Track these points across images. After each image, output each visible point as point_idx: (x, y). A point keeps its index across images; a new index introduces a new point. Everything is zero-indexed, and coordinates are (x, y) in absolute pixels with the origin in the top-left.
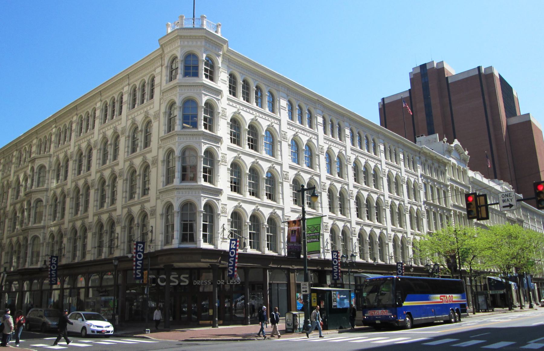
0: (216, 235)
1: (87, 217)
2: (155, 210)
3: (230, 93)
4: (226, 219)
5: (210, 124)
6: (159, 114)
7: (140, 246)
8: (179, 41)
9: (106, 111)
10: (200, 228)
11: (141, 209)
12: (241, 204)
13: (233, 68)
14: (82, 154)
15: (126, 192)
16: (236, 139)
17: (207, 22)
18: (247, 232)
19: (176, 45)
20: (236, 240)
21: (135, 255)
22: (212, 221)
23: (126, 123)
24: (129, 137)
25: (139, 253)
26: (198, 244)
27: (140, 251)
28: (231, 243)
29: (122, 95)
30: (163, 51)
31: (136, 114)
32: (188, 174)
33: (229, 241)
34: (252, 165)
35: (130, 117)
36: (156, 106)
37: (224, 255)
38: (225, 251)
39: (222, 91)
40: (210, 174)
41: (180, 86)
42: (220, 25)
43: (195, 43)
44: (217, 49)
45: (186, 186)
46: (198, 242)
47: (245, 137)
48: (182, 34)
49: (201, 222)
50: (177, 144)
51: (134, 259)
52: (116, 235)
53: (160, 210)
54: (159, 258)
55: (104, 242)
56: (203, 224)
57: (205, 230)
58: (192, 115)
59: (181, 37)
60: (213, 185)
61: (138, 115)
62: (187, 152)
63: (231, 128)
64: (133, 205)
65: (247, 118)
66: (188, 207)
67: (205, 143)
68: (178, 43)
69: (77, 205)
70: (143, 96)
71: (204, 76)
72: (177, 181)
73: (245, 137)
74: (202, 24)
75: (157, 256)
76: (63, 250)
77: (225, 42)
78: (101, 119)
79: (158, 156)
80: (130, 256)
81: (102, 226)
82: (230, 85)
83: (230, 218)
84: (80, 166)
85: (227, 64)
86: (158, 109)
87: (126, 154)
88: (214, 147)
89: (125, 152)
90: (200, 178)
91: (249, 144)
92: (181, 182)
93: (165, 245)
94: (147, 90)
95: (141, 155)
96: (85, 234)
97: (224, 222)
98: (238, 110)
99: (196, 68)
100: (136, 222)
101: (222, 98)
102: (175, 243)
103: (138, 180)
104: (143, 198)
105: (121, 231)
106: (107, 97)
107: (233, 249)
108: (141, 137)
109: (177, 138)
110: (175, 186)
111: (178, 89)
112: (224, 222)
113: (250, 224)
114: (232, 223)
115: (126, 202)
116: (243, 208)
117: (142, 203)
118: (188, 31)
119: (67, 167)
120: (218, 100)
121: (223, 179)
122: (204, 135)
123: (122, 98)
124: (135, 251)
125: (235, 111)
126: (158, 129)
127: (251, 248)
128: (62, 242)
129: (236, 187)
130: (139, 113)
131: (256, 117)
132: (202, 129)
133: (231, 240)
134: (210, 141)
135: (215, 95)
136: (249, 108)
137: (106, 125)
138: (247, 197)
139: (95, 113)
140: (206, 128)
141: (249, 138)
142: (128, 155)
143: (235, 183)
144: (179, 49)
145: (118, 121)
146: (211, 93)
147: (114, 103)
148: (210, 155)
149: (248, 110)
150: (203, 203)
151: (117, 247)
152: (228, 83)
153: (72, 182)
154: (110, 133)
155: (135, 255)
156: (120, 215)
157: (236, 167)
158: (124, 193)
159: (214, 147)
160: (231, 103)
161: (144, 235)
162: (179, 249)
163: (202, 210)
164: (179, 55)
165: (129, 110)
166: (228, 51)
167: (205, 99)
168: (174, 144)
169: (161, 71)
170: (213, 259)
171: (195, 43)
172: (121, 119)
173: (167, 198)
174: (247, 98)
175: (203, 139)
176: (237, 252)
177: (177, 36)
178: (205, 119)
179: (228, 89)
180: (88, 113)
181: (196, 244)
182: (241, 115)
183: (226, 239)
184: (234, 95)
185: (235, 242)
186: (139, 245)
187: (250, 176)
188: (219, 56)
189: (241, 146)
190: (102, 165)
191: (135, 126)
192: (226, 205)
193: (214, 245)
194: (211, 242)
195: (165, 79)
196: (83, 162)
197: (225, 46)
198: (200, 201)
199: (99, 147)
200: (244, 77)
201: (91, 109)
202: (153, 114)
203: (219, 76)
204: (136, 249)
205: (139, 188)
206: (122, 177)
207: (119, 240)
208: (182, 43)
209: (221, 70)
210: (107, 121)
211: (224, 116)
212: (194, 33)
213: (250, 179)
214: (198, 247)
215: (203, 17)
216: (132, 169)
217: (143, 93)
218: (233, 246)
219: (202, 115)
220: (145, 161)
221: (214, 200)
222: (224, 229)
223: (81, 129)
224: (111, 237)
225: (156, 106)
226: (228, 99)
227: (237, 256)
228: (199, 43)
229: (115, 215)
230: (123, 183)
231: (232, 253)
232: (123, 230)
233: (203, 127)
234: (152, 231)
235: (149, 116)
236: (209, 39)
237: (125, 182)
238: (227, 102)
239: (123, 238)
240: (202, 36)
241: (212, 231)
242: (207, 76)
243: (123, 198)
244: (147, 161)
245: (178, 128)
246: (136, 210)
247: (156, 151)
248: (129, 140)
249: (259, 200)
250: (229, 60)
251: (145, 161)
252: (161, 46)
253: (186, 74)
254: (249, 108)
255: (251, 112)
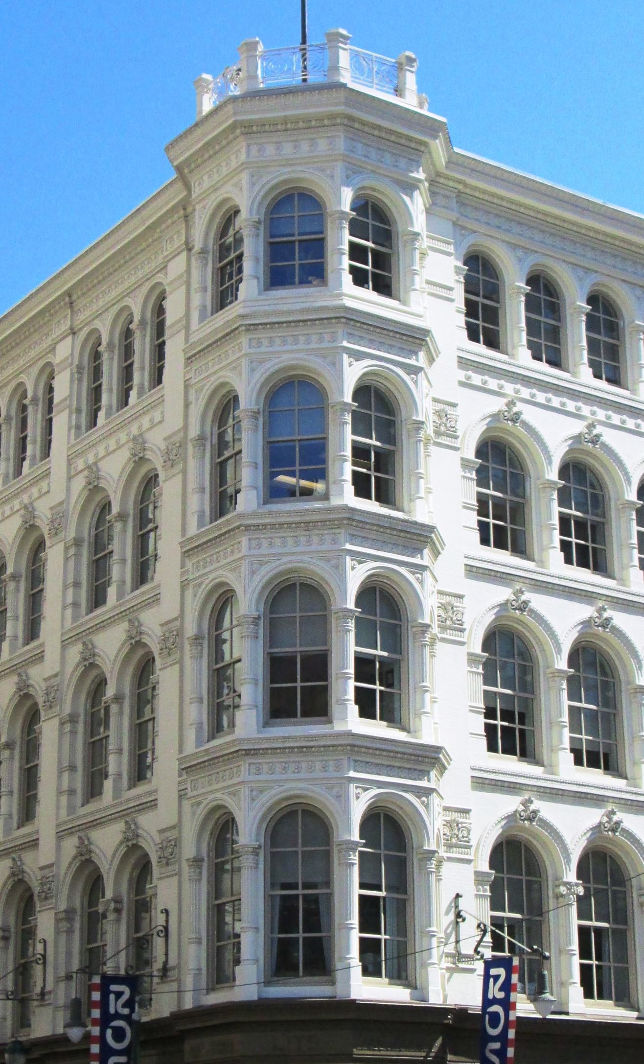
0: (420, 943)
1: (34, 844)
2: (176, 843)
3: (473, 336)
4: (468, 871)
5: (379, 475)
6: (182, 445)
7: (119, 995)
8: (242, 143)
9: (97, 373)
10: (348, 916)
11: (13, 874)
12: (536, 804)
13: (482, 229)
14: (106, 507)
15: (72, 768)
16: (504, 525)
17: (355, 56)
18: (566, 926)
19: (234, 164)
20: (506, 963)
21: (96, 1031)
22: (401, 882)
23: (68, 490)
24: (78, 542)
25: (116, 1023)
26: (339, 985)
27: (117, 1016)
28: (487, 976)
29: (162, 297)
30: (188, 187)
31: (101, 450)
32: (297, 689)
33: (480, 966)
34: (581, 634)
35: (80, 464)
36: (170, 413)
37: (459, 1027)
38: (461, 1013)
39: (427, 332)
40: (385, 687)
41: (252, 328)
42: (410, 61)
43: (305, 147)
44: (402, 163)
45: (285, 738)
46: (339, 975)
47: (546, 514)
48: (252, 120)
49: (350, 890)
50: (245, 566)
51: (95, 1049)
52: (160, 920)
53: (192, 843)
54: (188, 1045)
55: (110, 951)
56: (362, 898)
57: (369, 921)
58: (310, 440)
59: (248, 129)
60: (404, 729)
61: (108, 454)
62: (296, 599)
63: (482, 482)
64: (96, 824)
65: (552, 434)
66: (299, 828)
67: (361, 558)
68: (240, 153)
69: (96, 751)
70: (127, 373)
71: (347, 278)
72: (247, 721)
73: (546, 514)
74: (335, 68)
75: (184, 1035)
76: (38, 969)
77: (433, 128)
78: (79, 411)
79: (182, 616)
80: (75, 1034)
81: (95, 884)
82: (468, 303)
83: (484, 867)
84: (100, 568)
85: (454, 215)
86: (180, 424)
87: (69, 612)
88: (403, 570)
89: (64, 608)
90: (343, 703)
91: (565, 547)
92: (266, 725)
93: (210, 989)
94: (142, 346)
95: (121, 616)
96: (25, 921)
97: (455, 894)
98: (511, 404)
99: (316, 247)
100: (109, 894)
101: (431, 360)
102: (248, 983)
103: (112, 718)
104: (135, 792)
105: (57, 932)
106: (129, 293)
107: (495, 1001)
108: (124, 545)
109: (244, 540)
110: (241, 741)
111: (244, 339)
112: (455, 894)
113: (581, 891)
114: (496, 887)
115: (71, 809)
116: (544, 823)
117: (128, 815)
118: (273, 102)
119: (36, 578)
120: (415, 371)
121: (449, 700)
122: (354, 523)
123: (160, 311)
124: (96, 1013)
125: (494, 409)
126: (180, 506)
127: (588, 994)
128: (28, 934)
129: (511, 730)
130: (112, 443)
131: (591, 426)
132: (348, 497)
133: (489, 965)
134: (382, 545)
135: (401, 351)
136: (558, 390)
137: (23, 481)
138: (562, 776)
139: (50, 390)
140: (362, 490)
141: (564, 520)
142: (75, 618)
143: (507, 715)
144: (245, 177)
145: (36, 481)
146: (380, 346)
147: (128, 333)
148: (384, 605)
149: (556, 402)
150: (358, 808)
151: (43, 994)
152: (459, 295)
153: (65, 645)
154: (114, 469)
155: (96, 1031)
156: (51, 866)
157: (508, 651)
158: (66, 776)
159: (403, 570)
160: (477, 379)
161: (140, 945)
162: (262, 1006)
163: (355, 836)
164: (247, 200)
165: (77, 436)
166: (454, 161)
167: (352, 373)
168: (235, 568)
169: (188, 271)
170: (410, 1046)
171: (305, 147)
172: (47, 474)
173: (214, 791)
174: (548, 345)
175: (353, 538)
176: (512, 1016)
177: (233, 127)
178: (360, 453)
179: (462, 319)
180: (126, 314)
181: (333, 983)
182: (525, 425)
183: (470, 958)
184: (492, 342)
185: (501, 971)
186: (114, 988)
187: (572, 681)
188: (410, 187)
189: (530, 558)
190: (90, 610)
191: (98, 498)
192: (466, 812)
193: (410, 985)
194: (400, 974)
195: (202, 298)
196: (115, 546)
197: (437, 146)
198: (343, 799)
199: (71, 534)
200: (531, 261)
201: (35, 370)
202: (163, 446)
203: (414, 273)
204: (104, 1004)
205: (120, 751)
206: (57, 709)
207: (50, 969)
208: (254, 150)
209: (424, 243)
210: (101, 415)
211: (447, 433)
212: (296, 108)
213: (573, 695)
214: (339, 992)
215: (334, 39)
216: (94, 673)
217: (125, 361)
218: (495, 992)
219: (344, 438)
220: (136, 643)
221: (409, 796)
222: (458, 915)
223: (96, 393)
224: (137, 929)
225: (170, 413)
226: (464, 363)
227: (512, 1034)
228: (322, 145)
229: (33, 864)
230: (61, 734)
231: (495, 1017)
232: (64, 925)
233: (349, 488)
234: (166, 928)
235: (149, 455)
236: (364, 123)
237: (67, 728)
238: (461, 375)
239: (62, 957)
240: (332, 116)
241: (402, 928)
242: (359, 278)
243: (60, 793)
244: (146, 639)
245: (248, 501)
246: (107, 842)
247: (171, 601)
248: (77, 555)
249: (620, 783)
250: (457, 199)
251: (136, 643)
252: (179, 169)
253: (277, 278)
254: (558, 390)
255: (571, 406)
